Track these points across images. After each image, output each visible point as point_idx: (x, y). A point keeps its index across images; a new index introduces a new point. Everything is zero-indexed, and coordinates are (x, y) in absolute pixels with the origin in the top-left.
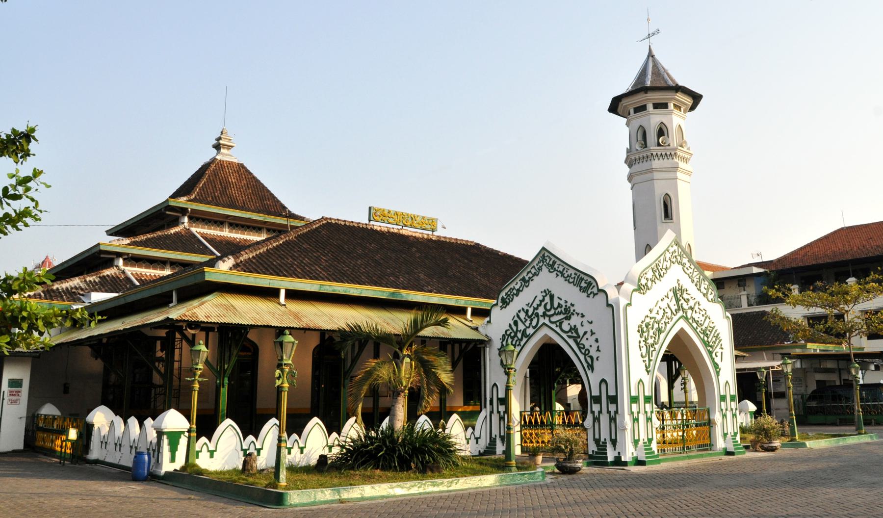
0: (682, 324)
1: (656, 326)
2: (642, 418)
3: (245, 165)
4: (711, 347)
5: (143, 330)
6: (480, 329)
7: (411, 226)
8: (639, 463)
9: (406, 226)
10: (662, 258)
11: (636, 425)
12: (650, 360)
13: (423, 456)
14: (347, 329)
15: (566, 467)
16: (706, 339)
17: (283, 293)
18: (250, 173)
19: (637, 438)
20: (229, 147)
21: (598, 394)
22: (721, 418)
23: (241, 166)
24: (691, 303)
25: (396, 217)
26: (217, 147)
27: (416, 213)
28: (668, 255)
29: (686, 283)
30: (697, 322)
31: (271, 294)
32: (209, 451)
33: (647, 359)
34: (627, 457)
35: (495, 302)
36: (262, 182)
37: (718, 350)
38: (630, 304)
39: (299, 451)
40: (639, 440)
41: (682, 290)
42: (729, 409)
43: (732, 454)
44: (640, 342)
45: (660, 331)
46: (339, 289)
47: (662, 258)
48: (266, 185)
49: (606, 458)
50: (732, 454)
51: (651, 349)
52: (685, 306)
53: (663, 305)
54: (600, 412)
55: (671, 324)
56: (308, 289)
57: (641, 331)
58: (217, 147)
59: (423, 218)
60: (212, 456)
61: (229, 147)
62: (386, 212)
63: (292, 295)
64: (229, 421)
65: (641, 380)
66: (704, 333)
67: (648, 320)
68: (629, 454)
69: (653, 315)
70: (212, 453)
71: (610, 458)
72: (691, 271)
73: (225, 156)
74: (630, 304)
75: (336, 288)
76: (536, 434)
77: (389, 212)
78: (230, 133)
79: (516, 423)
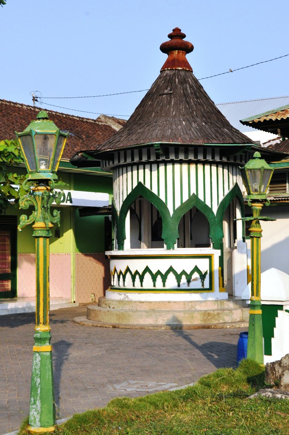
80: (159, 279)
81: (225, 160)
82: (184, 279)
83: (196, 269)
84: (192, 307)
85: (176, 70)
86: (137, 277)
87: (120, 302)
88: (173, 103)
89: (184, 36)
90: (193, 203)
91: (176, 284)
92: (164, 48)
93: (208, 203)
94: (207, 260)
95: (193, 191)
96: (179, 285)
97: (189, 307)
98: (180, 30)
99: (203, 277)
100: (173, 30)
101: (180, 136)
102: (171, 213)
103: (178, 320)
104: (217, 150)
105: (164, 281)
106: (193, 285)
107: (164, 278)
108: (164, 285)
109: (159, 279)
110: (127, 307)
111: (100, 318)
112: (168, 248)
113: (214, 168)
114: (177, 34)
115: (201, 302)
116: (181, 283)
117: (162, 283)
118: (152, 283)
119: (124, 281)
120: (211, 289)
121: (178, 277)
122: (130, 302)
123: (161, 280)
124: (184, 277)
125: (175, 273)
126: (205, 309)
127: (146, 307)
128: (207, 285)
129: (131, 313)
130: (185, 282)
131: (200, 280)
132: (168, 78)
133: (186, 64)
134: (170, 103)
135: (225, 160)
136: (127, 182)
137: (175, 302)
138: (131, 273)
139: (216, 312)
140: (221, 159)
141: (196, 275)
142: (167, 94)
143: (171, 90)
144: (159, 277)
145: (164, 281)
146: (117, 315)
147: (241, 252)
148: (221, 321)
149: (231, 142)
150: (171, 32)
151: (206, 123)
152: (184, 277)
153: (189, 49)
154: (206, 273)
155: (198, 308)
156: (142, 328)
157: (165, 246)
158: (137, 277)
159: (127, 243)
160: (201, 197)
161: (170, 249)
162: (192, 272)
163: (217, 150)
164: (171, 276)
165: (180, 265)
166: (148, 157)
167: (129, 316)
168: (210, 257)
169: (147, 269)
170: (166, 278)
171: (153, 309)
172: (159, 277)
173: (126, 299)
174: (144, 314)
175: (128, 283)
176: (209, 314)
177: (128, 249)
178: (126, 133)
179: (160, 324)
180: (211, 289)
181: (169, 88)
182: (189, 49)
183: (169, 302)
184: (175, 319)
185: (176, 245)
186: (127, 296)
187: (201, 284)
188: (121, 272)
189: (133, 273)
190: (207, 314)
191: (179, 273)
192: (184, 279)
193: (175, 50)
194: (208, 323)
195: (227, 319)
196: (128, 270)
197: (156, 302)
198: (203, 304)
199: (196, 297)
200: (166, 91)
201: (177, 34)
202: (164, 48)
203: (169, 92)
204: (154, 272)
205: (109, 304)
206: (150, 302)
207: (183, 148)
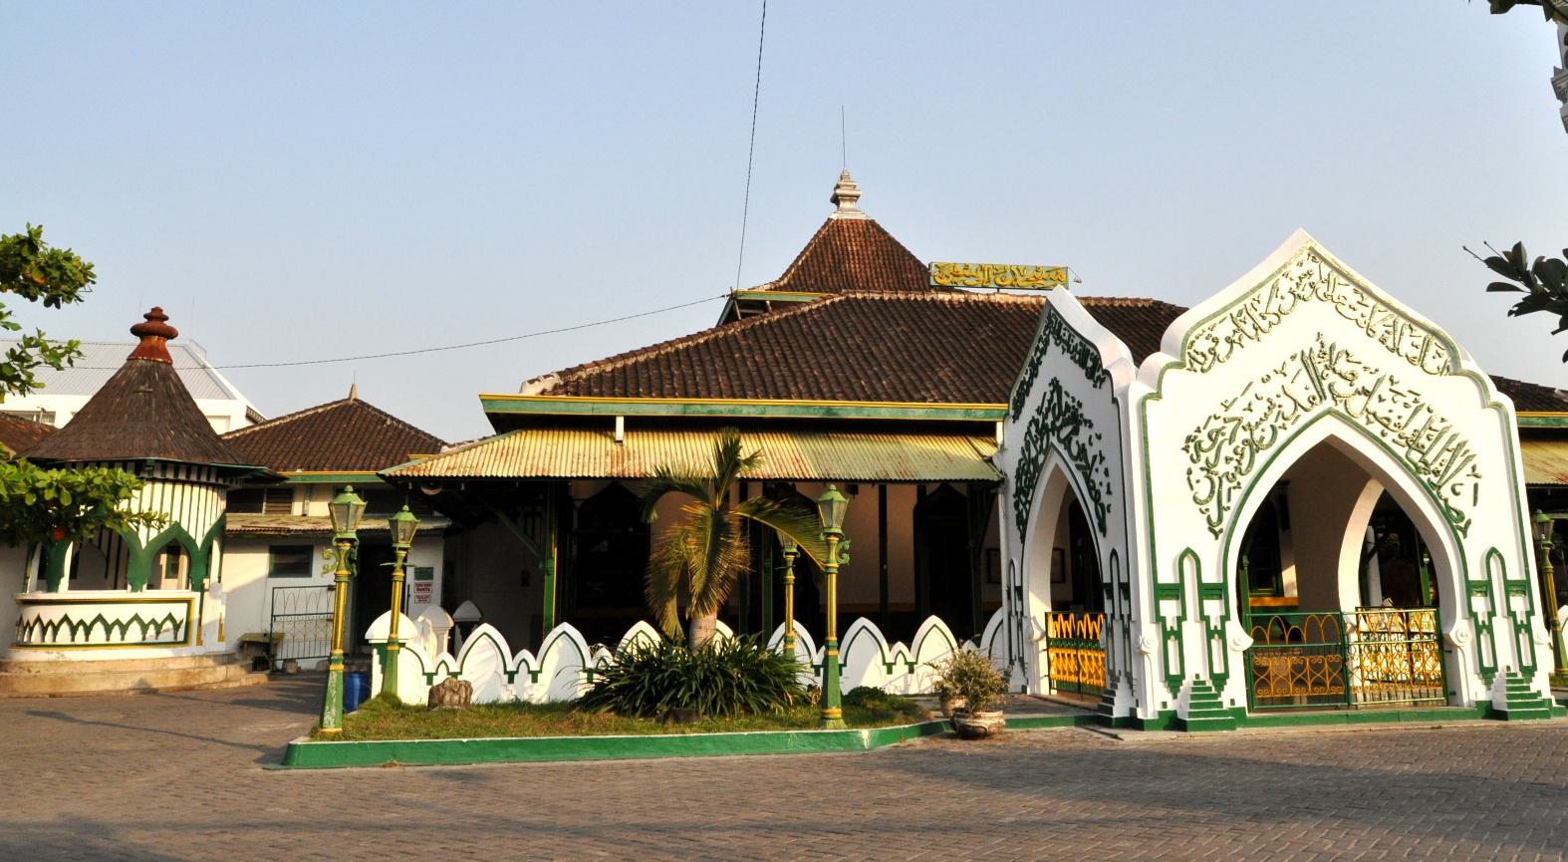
0: (1328, 428)
1: (1242, 435)
2: (1502, 626)
3: (877, 222)
4: (1436, 473)
5: (952, 485)
6: (995, 461)
7: (1013, 287)
8: (1174, 722)
9: (1002, 287)
10: (1267, 288)
11: (1484, 639)
12: (1221, 508)
13: (753, 688)
14: (654, 475)
15: (965, 727)
16: (1416, 456)
17: (620, 423)
18: (884, 233)
19: (1174, 670)
20: (854, 198)
21: (1126, 581)
22: (1471, 635)
23: (872, 223)
24: (1365, 381)
25: (980, 274)
26: (836, 200)
27: (1022, 263)
28: (1285, 285)
29: (1345, 335)
30: (1385, 422)
31: (601, 425)
32: (906, 663)
33: (1213, 505)
34: (1148, 712)
35: (1004, 406)
36: (903, 244)
37: (1463, 477)
38: (1157, 396)
39: (906, 668)
40: (1495, 669)
41: (1330, 354)
42: (1117, 616)
43: (1501, 715)
44: (1190, 472)
45: (1254, 446)
46: (722, 408)
47: (1267, 288)
48: (908, 248)
49: (1110, 711)
50: (1501, 715)
51: (1226, 485)
52: (1342, 387)
53: (1271, 390)
54: (1181, 619)
55: (1292, 429)
56: (663, 413)
57: (1192, 444)
58: (836, 200)
59: (1037, 269)
60: (535, 680)
61: (854, 198)
62: (960, 269)
63: (635, 424)
64: (934, 620)
65: (1493, 551)
66: (1412, 444)
67: (1215, 425)
68: (1156, 698)
69: (1236, 411)
70: (534, 676)
71: (1119, 711)
72: (1367, 312)
73: (849, 212)
74: (1157, 396)
75: (714, 408)
76: (1089, 657)
77: (966, 267)
78: (855, 177)
79: (1037, 634)
80: (116, 630)
81: (220, 482)
82: (152, 630)
83: (170, 617)
84: (164, 665)
85: (154, 361)
86: (50, 629)
87: (50, 663)
88: (154, 406)
89: (166, 318)
90: (174, 534)
91: (141, 636)
92: (136, 330)
93: (192, 534)
94: (185, 605)
95: (175, 518)
96: (144, 638)
97: (160, 667)
98: (162, 311)
99: (177, 627)
100: (153, 310)
101: (173, 450)
102: (144, 545)
103: (146, 683)
104: (214, 471)
105: (123, 634)
106: (163, 638)
107: (88, 630)
108: (87, 639)
109: (116, 630)
110: (64, 670)
111: (16, 686)
112: (134, 590)
113: (203, 490)
114: (156, 315)
115: (175, 658)
116: (147, 636)
117: (120, 637)
118: (104, 636)
119: (31, 634)
120: (186, 641)
121: (144, 628)
122: (70, 662)
123: (119, 632)
124: (152, 627)
125: (70, 623)
126: (181, 667)
127: (96, 668)
128: (181, 638)
129: (76, 676)
130: (153, 634)
131: (172, 632)
132: (144, 370)
133: (166, 355)
134: (150, 404)
135: (220, 482)
136: (858, 633)
137: (142, 660)
138: (41, 623)
139: (197, 670)
140: (217, 480)
141: (168, 625)
142: (144, 392)
143: (149, 387)
144: (81, 628)
145: (123, 634)
146: (51, 680)
147: (215, 597)
148: (202, 682)
149: (234, 462)
150: (149, 311)
151: (199, 435)
152: (152, 627)
153: (171, 334)
154: (182, 622)
155: (171, 666)
156: (99, 694)
157: (129, 587)
158: (50, 629)
159: (65, 582)
160: (184, 526)
161: (136, 591)
162: (164, 621)
163: (214, 471)
164: (135, 626)
165: (148, 613)
166: (445, 546)
167: (73, 680)
168: (189, 602)
169: (66, 619)
170: (91, 629)
171: (108, 671)
172: (81, 628)
173: (61, 659)
174: (98, 676)
175: (36, 637)
176: (188, 673)
177: (64, 590)
178: (1086, 704)
179: (121, 688)
180: (186, 641)
181: (147, 385)
182: (171, 334)
183: (133, 660)
184: (142, 681)
185: (145, 586)
186: (62, 655)
187: (173, 636)
188: (28, 623)
189: (45, 624)
190: (185, 673)
191: (146, 622)
192: (152, 630)
193: (154, 334)
194: (186, 684)
195: (209, 678)
196: (38, 619)
197: (111, 661)
198: (178, 661)
199: (167, 652)
200: (142, 388)
201: (156, 315)
202: (136, 330)
203: (148, 390)
204: (110, 622)
205: (28, 667)
206: (105, 661)
207: (173, 465)
